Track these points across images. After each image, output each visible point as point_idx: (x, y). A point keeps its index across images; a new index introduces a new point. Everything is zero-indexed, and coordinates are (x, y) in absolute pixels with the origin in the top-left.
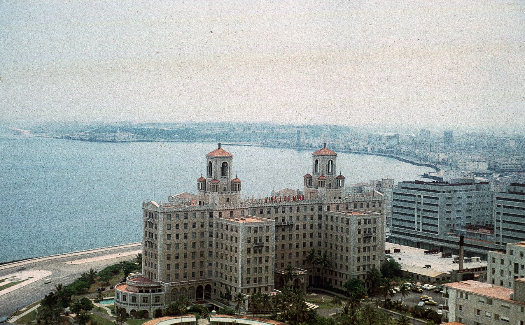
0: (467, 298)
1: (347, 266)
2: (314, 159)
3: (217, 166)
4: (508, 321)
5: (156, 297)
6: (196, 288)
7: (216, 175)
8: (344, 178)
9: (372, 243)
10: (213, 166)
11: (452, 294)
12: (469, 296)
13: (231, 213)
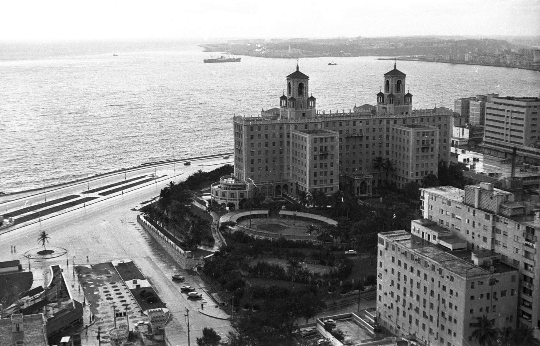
0: (435, 200)
1: (407, 172)
2: (385, 80)
3: (393, 83)
4: (460, 219)
5: (241, 194)
6: (275, 187)
7: (294, 94)
8: (412, 96)
9: (430, 153)
10: (390, 83)
11: (426, 196)
12: (437, 198)
13: (306, 126)
